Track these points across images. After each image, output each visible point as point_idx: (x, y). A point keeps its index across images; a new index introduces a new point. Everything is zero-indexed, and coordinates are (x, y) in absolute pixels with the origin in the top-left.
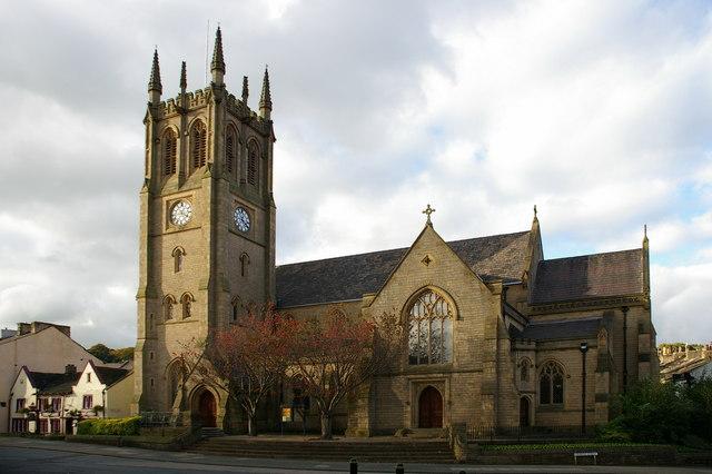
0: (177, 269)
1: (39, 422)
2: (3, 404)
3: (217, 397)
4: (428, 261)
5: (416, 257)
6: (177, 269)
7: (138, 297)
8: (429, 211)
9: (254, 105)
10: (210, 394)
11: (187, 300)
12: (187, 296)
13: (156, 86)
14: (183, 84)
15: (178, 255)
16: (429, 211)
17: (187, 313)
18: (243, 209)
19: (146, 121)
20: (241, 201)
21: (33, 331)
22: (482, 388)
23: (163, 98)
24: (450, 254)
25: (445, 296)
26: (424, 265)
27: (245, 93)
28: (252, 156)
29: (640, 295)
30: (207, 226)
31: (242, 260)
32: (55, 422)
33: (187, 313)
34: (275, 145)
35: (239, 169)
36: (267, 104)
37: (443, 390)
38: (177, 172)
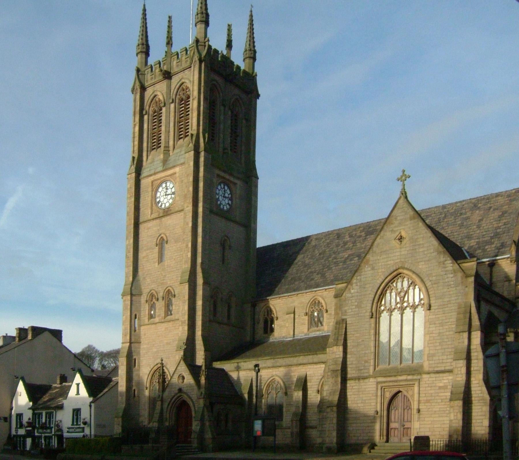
0: (161, 258)
1: (34, 438)
2: (5, 419)
3: (193, 409)
4: (401, 239)
5: (388, 235)
6: (161, 258)
7: (123, 295)
8: (404, 177)
9: (238, 58)
10: (188, 405)
11: (169, 296)
12: (152, 295)
13: (145, 50)
14: (169, 43)
15: (162, 243)
16: (404, 177)
17: (168, 311)
18: (225, 184)
19: (133, 90)
20: (222, 174)
21: (30, 337)
22: (452, 393)
23: (151, 61)
24: (7, 435)
25: (417, 280)
26: (396, 243)
27: (229, 45)
28: (235, 118)
29: (292, 433)
30: (189, 208)
31: (223, 245)
32: (48, 439)
33: (168, 311)
34: (259, 102)
35: (222, 136)
36: (252, 55)
37: (413, 396)
38: (162, 148)
